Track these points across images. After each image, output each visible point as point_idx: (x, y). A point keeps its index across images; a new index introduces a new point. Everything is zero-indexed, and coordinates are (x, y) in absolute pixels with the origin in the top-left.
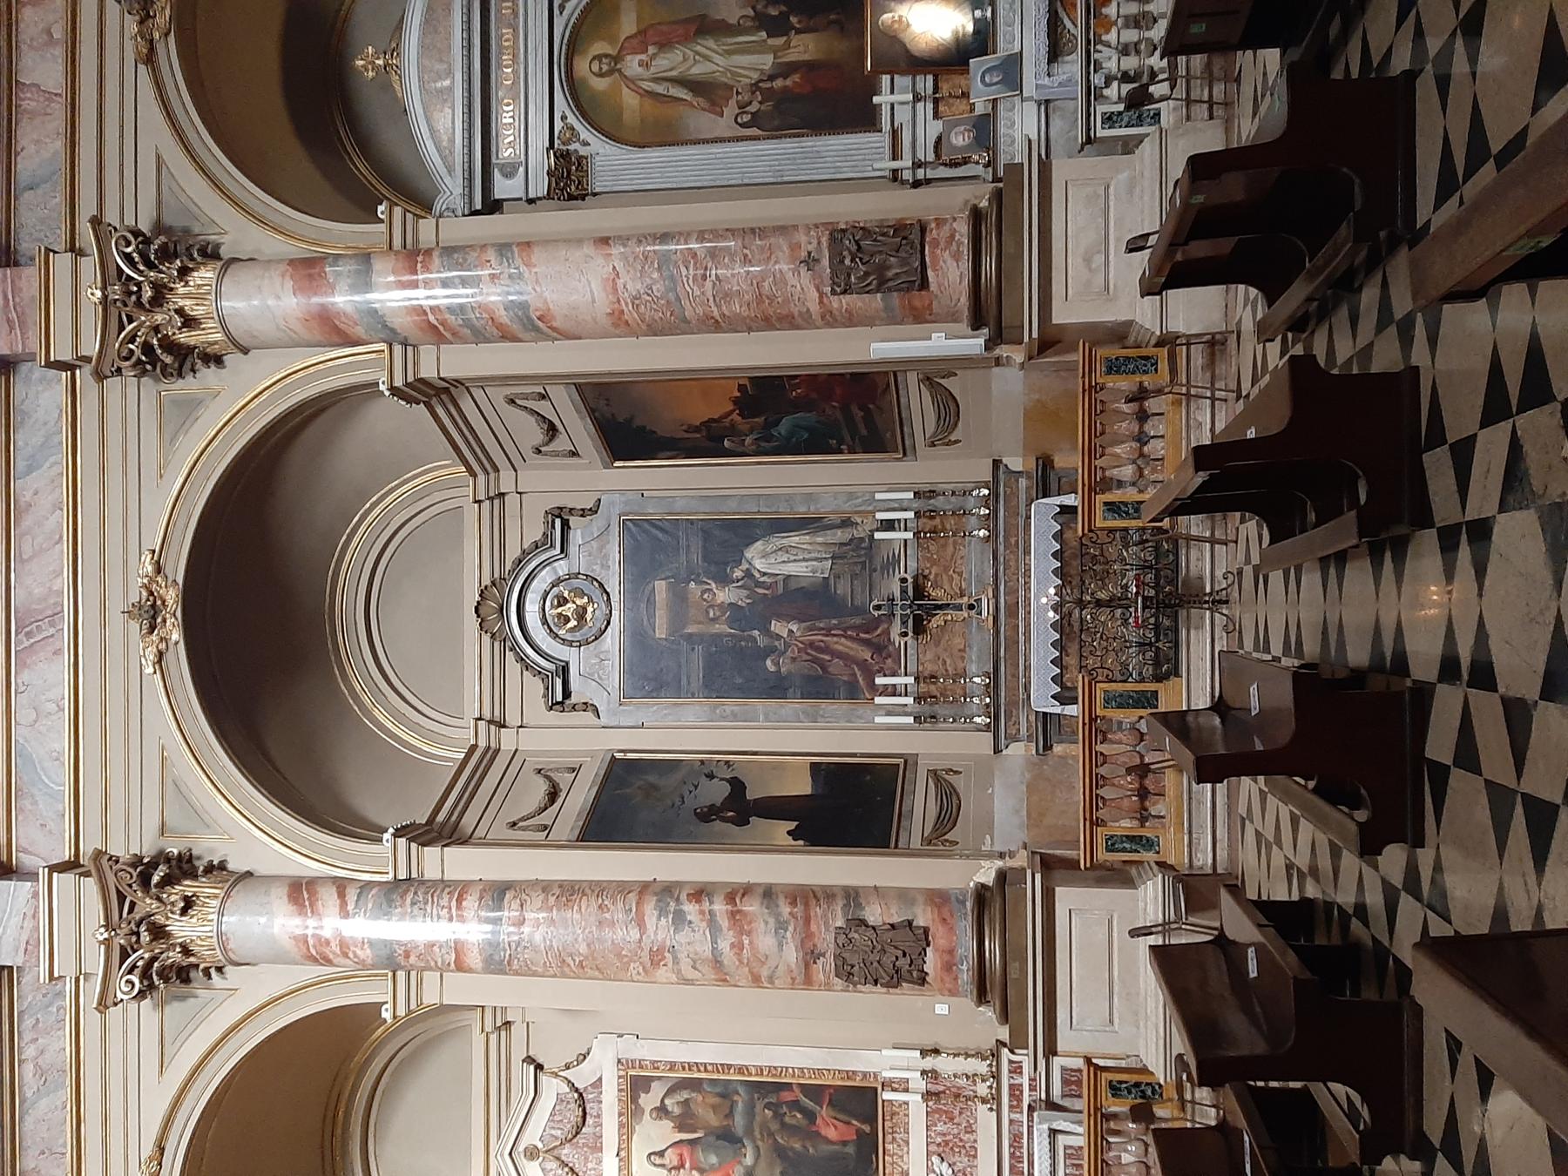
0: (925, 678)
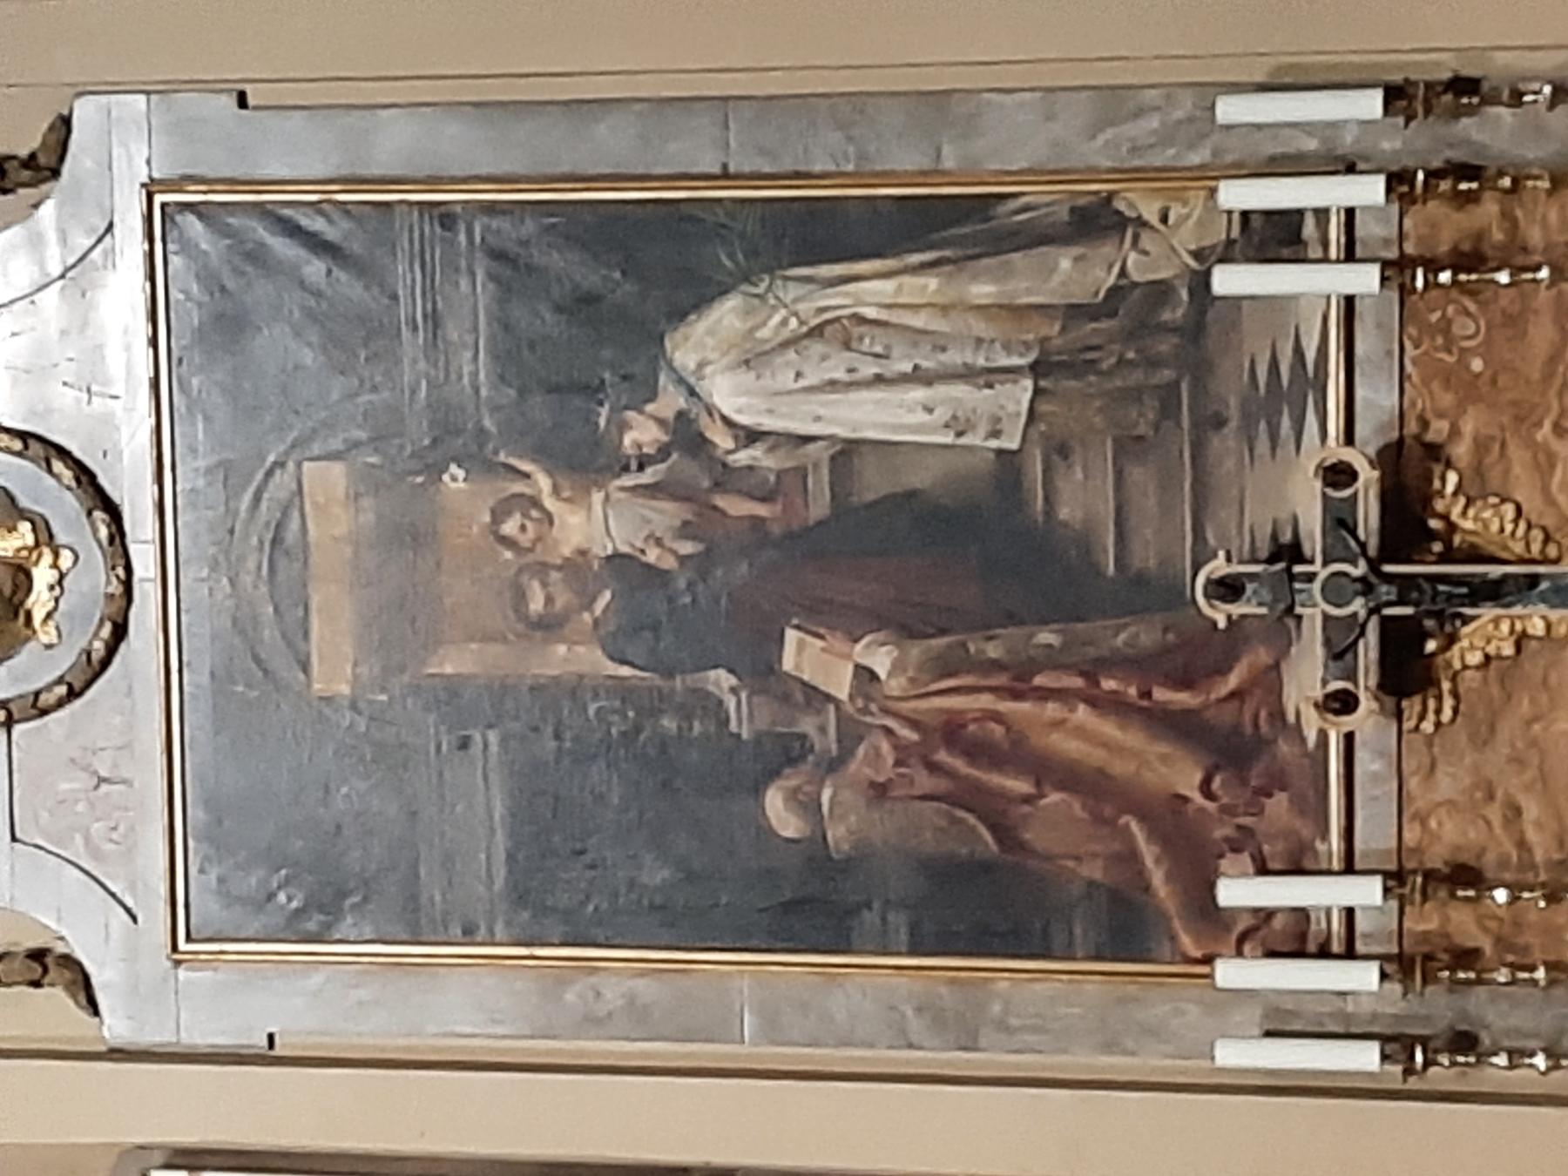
0: (1429, 875)
